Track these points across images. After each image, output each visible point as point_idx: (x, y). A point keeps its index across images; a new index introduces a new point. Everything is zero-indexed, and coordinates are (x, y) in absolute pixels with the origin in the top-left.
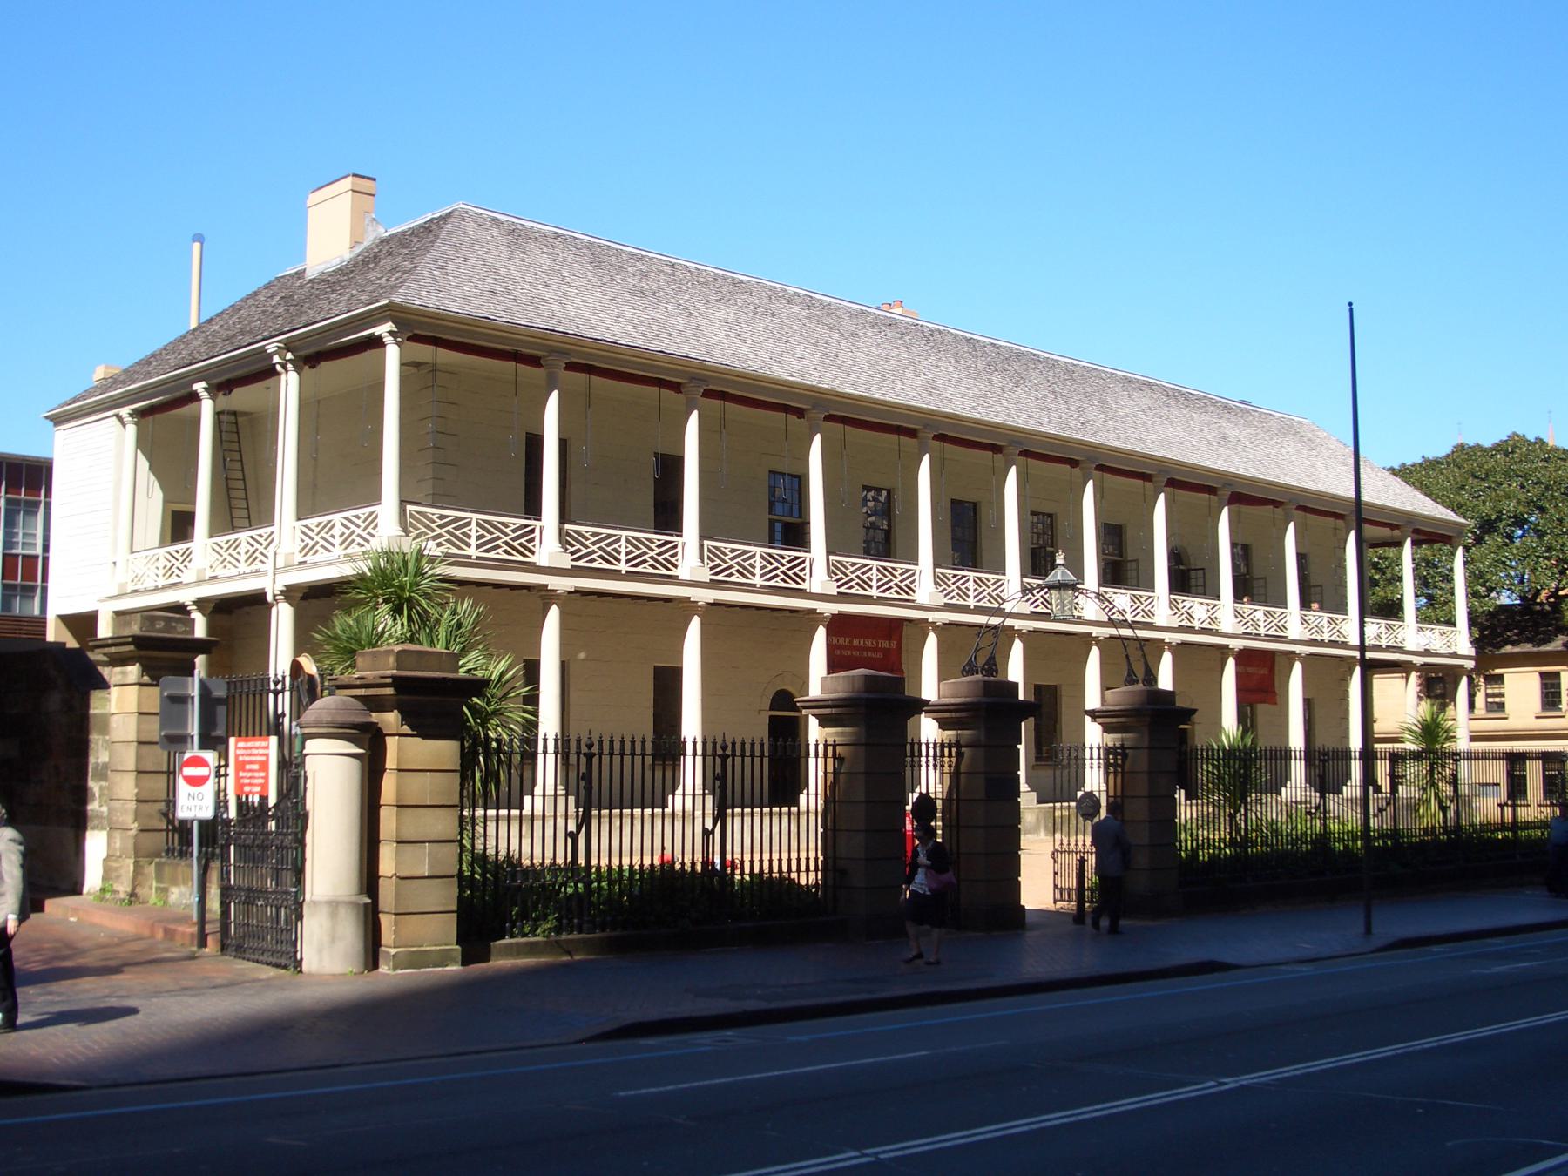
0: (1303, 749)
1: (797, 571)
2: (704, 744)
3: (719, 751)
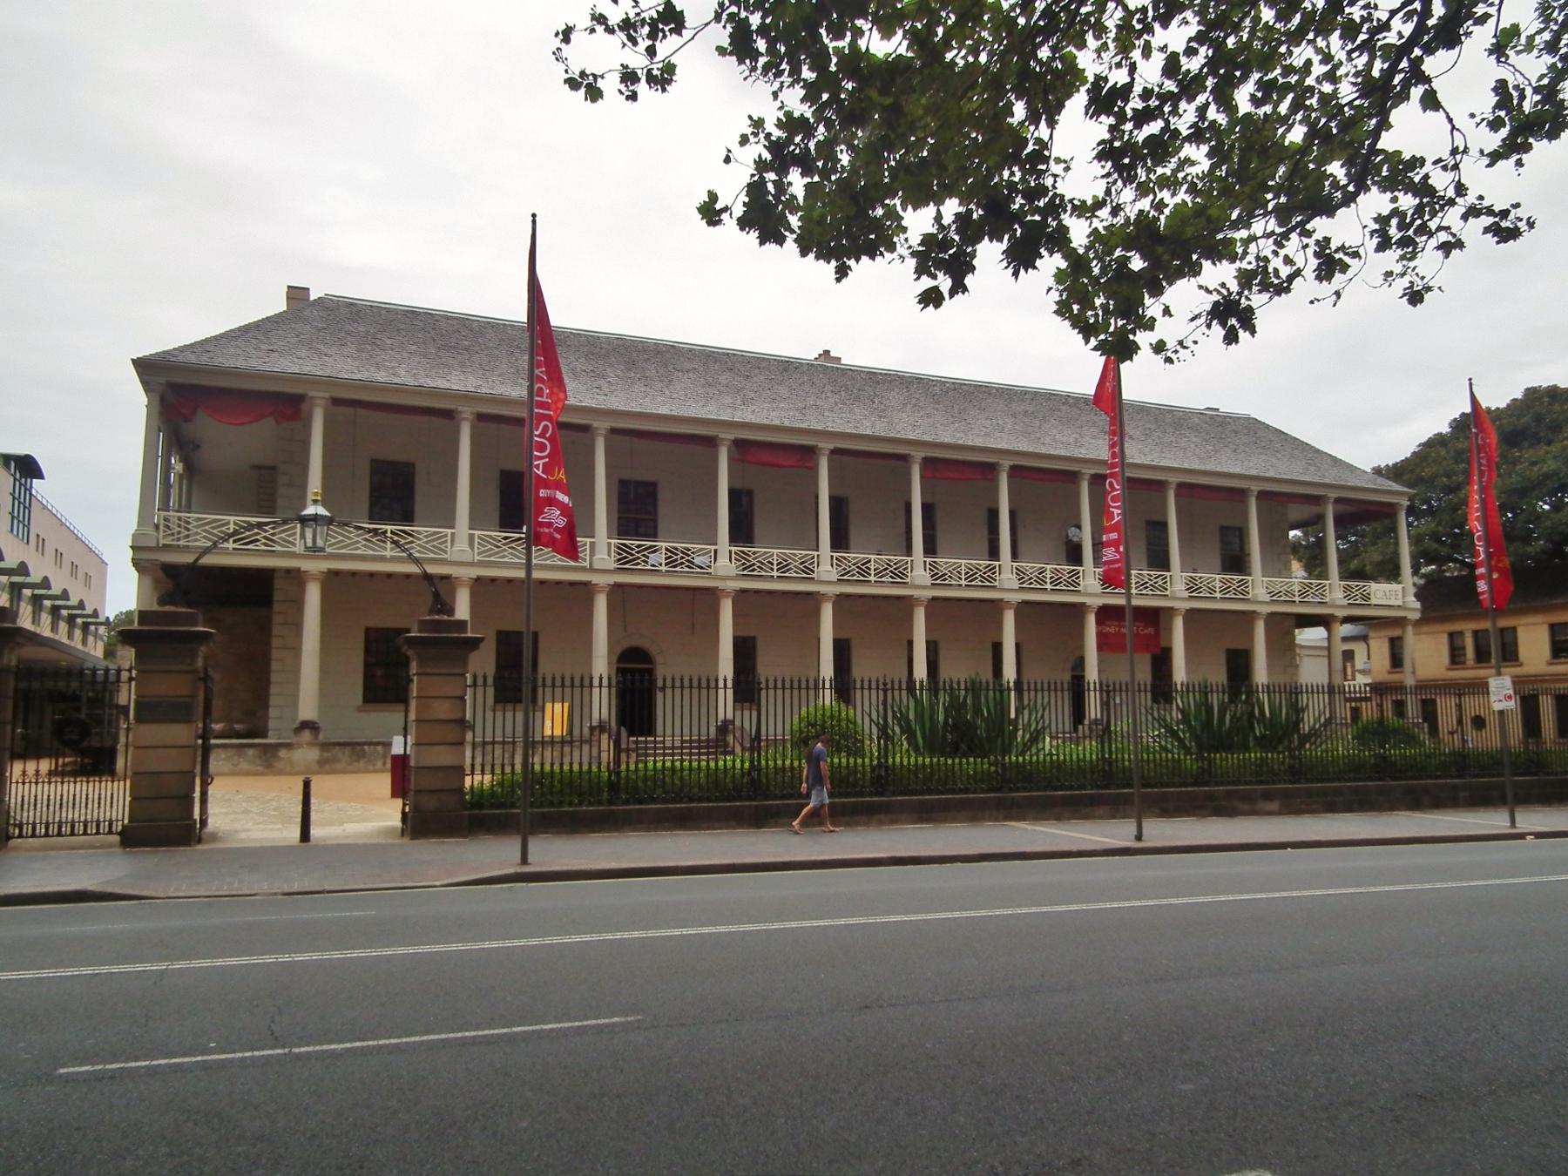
0: (1149, 683)
1: (1074, 579)
2: (1101, 684)
3: (1105, 688)
